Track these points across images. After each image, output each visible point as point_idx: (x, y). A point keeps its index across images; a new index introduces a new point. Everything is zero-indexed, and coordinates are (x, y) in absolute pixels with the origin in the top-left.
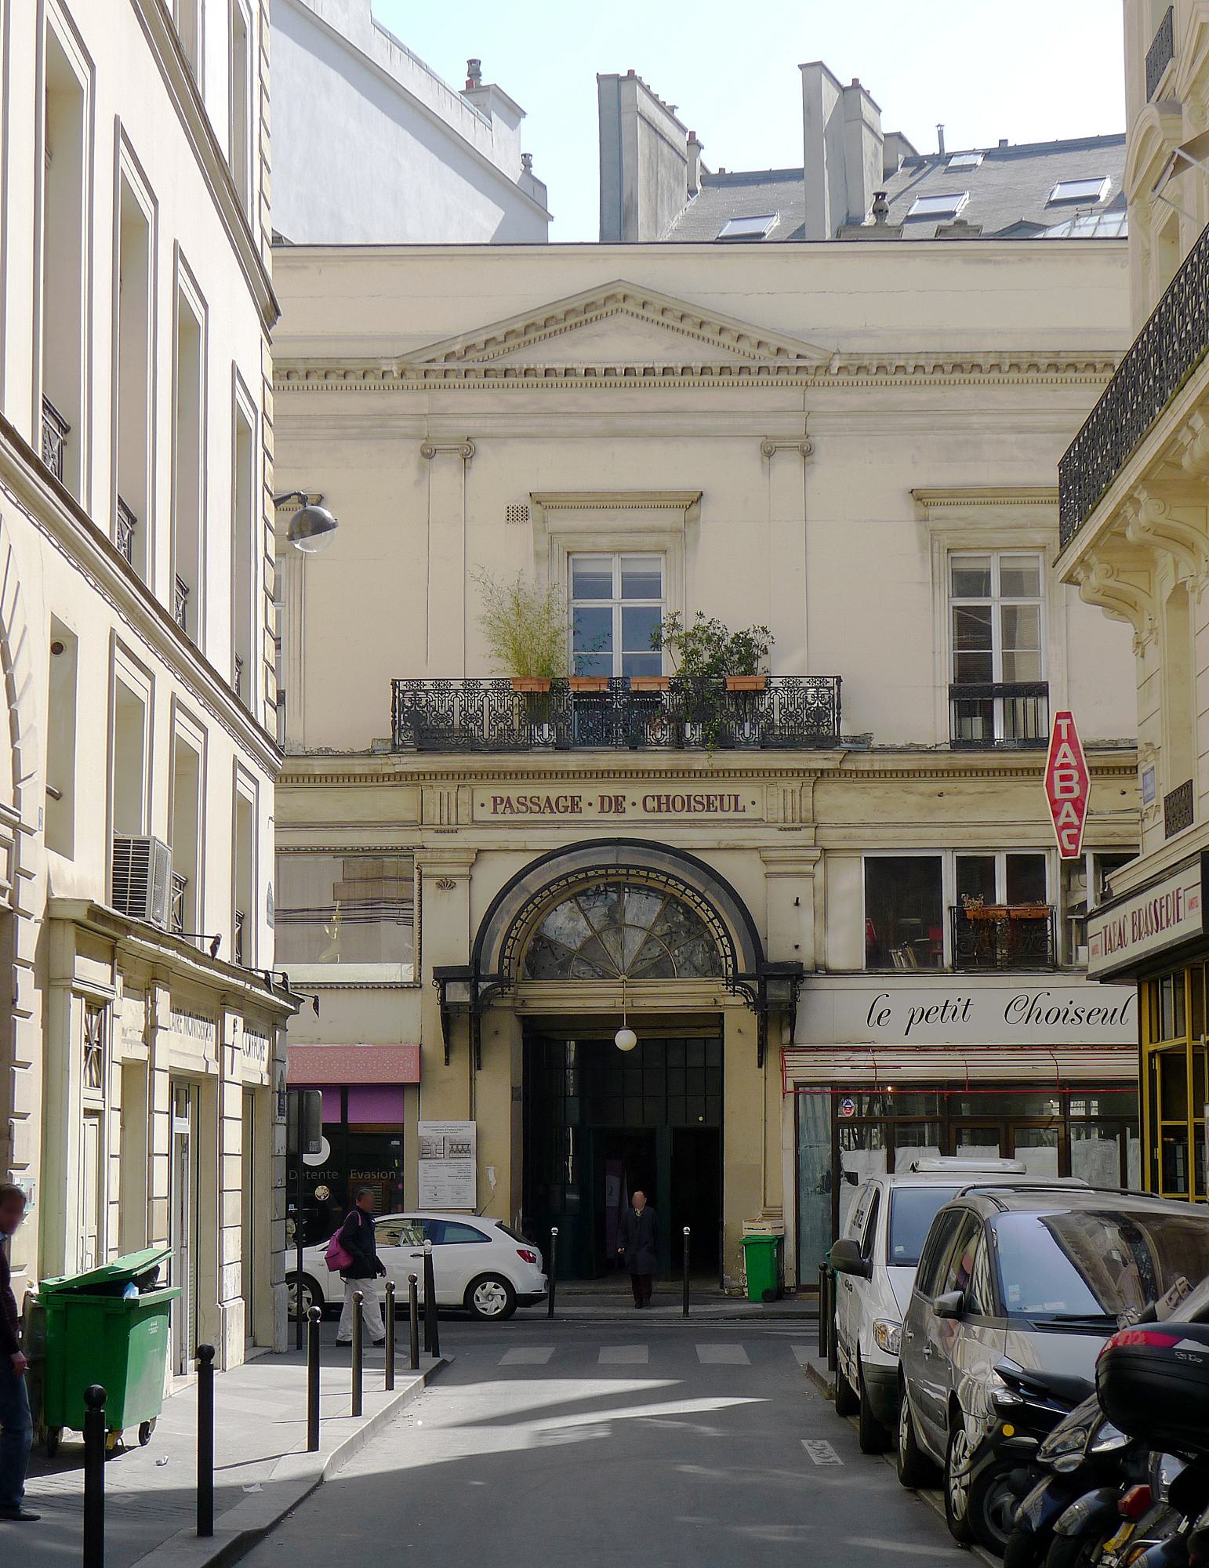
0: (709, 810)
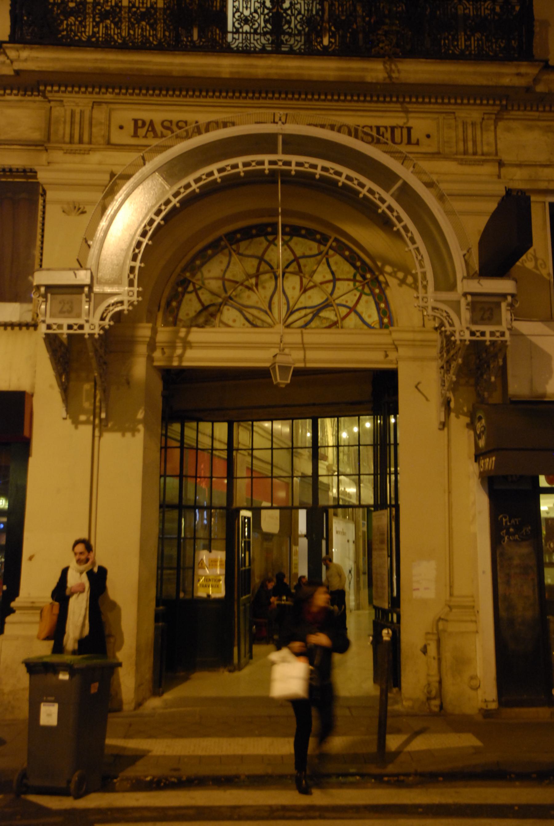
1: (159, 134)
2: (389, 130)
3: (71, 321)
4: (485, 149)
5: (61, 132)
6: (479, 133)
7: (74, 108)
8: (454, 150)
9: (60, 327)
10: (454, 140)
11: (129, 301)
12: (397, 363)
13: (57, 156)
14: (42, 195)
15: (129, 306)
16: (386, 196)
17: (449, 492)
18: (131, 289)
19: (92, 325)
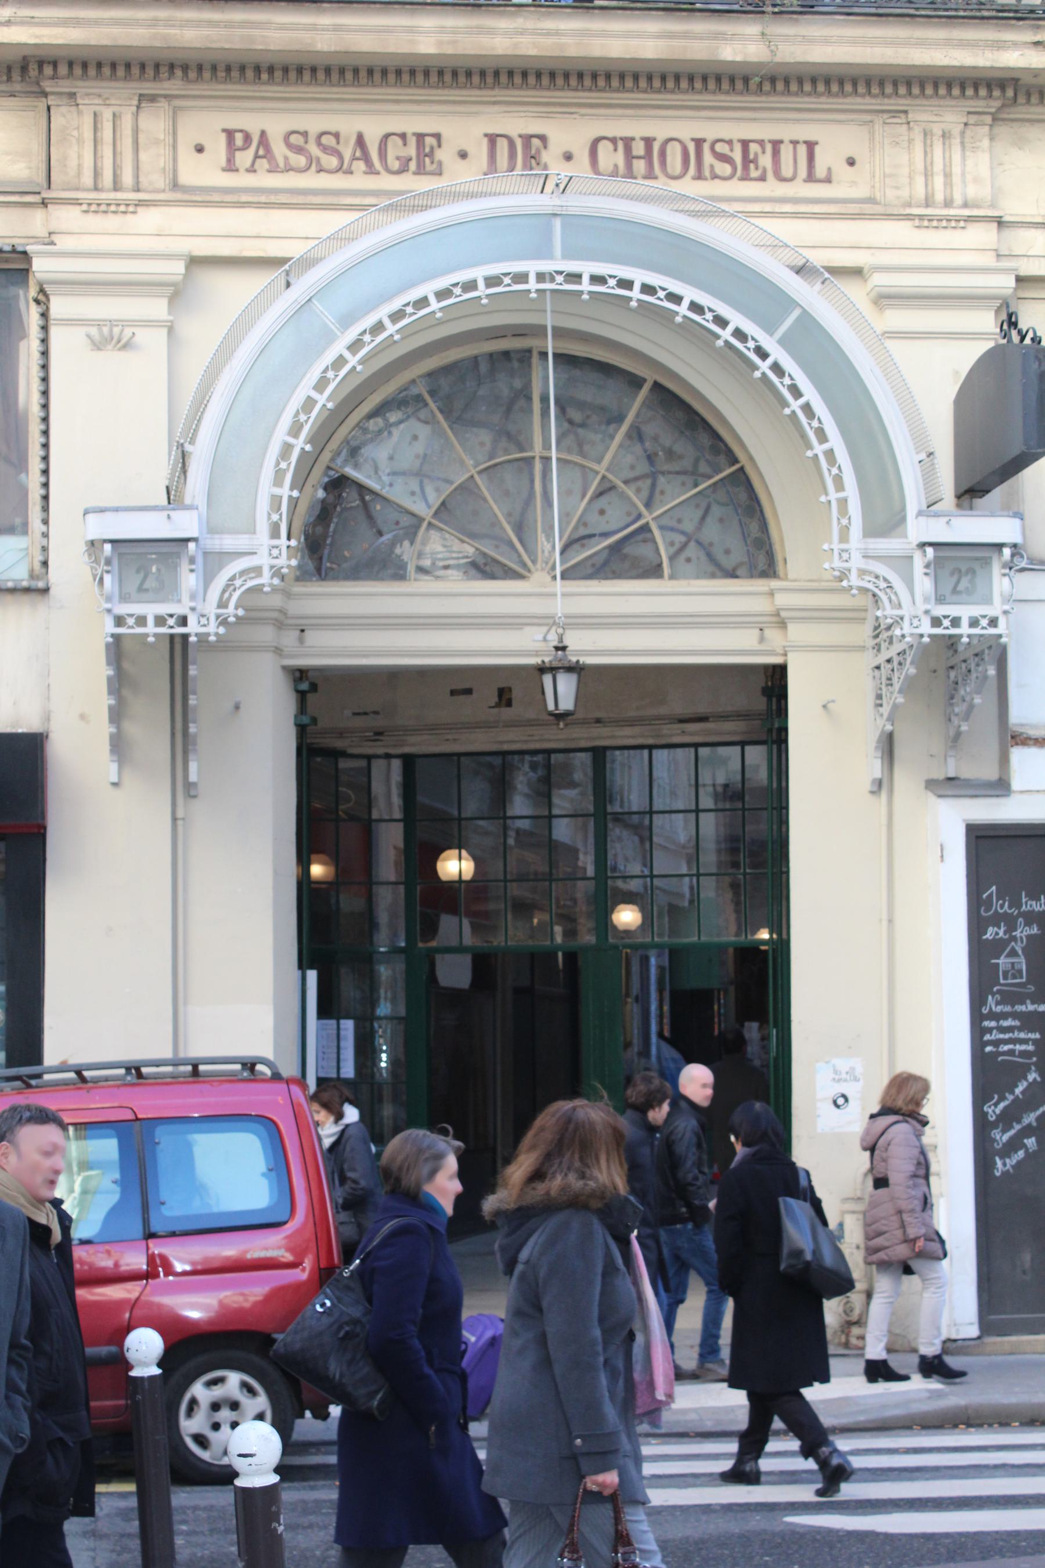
0: (745, 178)
1: (282, 164)
2: (769, 148)
3: (163, 609)
4: (972, 191)
5: (73, 163)
6: (957, 156)
7: (97, 108)
8: (905, 193)
9: (141, 621)
10: (906, 171)
11: (272, 567)
12: (785, 655)
13: (65, 217)
14: (37, 302)
15: (272, 578)
16: (768, 343)
17: (890, 921)
18: (275, 542)
19: (203, 616)
